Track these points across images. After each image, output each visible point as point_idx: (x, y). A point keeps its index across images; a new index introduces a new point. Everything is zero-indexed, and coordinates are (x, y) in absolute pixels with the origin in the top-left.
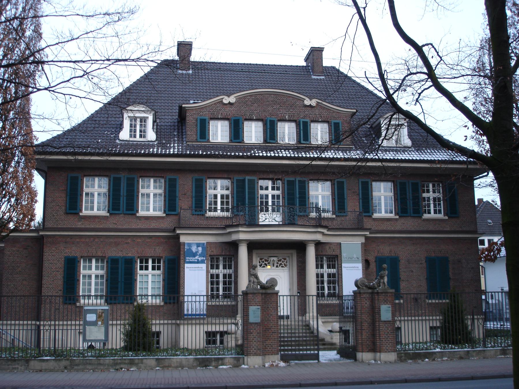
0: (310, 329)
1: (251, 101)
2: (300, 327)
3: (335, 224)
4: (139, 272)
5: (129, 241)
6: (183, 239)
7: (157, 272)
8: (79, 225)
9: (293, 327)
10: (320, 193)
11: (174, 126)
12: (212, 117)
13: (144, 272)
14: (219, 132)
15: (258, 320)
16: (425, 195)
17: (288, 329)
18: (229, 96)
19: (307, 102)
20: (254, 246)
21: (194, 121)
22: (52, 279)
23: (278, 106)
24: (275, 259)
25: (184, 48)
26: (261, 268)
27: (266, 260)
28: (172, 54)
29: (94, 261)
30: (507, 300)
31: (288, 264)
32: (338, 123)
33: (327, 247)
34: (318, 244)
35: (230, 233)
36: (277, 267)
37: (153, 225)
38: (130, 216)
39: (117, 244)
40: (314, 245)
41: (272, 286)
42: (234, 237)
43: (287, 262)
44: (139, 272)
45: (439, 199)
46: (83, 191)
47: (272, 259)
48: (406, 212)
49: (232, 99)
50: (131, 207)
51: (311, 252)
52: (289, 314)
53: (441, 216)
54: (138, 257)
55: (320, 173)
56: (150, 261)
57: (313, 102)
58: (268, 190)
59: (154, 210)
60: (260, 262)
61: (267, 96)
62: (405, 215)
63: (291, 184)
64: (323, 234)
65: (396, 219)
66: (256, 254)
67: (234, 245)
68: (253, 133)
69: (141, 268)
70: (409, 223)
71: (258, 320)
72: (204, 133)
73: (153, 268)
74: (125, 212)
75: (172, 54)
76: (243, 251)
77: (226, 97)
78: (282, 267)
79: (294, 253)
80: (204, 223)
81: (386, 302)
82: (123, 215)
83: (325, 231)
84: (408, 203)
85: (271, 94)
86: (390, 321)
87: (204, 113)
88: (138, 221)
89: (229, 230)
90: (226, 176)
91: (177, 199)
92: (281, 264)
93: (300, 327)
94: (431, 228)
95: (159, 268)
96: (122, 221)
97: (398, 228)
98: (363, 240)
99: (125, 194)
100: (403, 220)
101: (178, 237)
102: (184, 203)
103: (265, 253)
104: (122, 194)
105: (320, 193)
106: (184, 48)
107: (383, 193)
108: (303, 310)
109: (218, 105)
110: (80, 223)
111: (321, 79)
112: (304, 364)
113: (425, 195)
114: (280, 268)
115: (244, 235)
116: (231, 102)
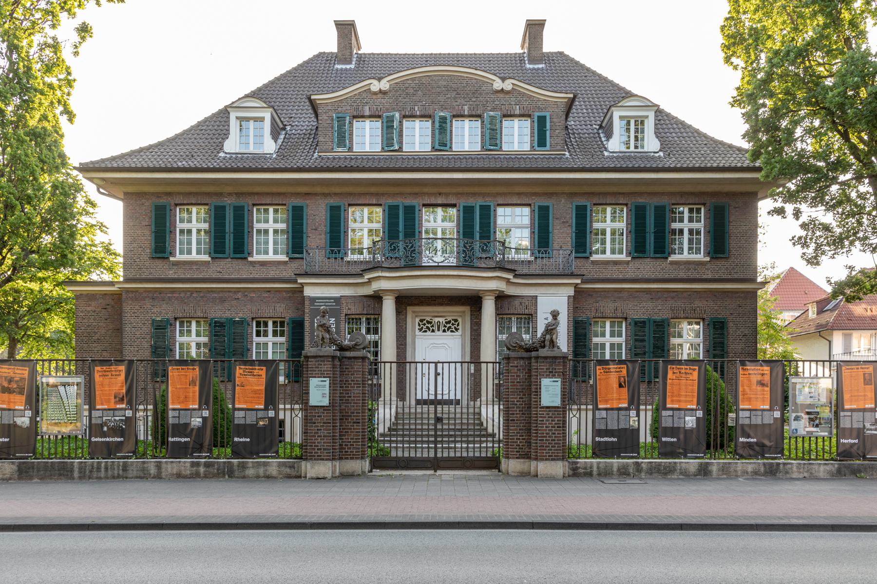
0: (480, 419)
1: (413, 88)
2: (471, 416)
3: (535, 269)
4: (256, 339)
5: (239, 295)
6: (309, 292)
7: (280, 339)
8: (171, 274)
9: (419, 416)
10: (514, 226)
11: (310, 134)
12: (355, 114)
13: (262, 339)
14: (367, 138)
15: (326, 402)
16: (676, 225)
17: (416, 419)
18: (380, 79)
19: (498, 85)
20: (405, 301)
21: (329, 122)
22: (136, 349)
23: (454, 94)
24: (441, 320)
25: (346, 30)
26: (421, 333)
27: (428, 322)
28: (331, 45)
29: (194, 324)
30: (629, 244)
31: (460, 327)
32: (545, 117)
33: (517, 302)
34: (501, 298)
35: (370, 281)
36: (444, 331)
37: (272, 273)
38: (240, 261)
39: (223, 300)
40: (493, 298)
41: (356, 345)
42: (376, 286)
43: (458, 325)
44: (256, 339)
45: (698, 233)
46: (175, 227)
47: (437, 320)
48: (643, 251)
49: (384, 85)
50: (241, 249)
51: (489, 307)
52: (459, 397)
53: (700, 257)
54: (253, 319)
55: (513, 194)
56: (270, 324)
57: (508, 85)
58: (440, 223)
59: (276, 252)
60: (419, 325)
61: (437, 78)
62: (641, 255)
63: (468, 212)
64: (508, 281)
65: (628, 263)
66: (413, 312)
67: (377, 298)
68: (417, 137)
69: (258, 335)
70: (648, 267)
71: (326, 402)
72: (343, 138)
73: (275, 334)
74: (232, 255)
75: (331, 45)
76: (389, 307)
77: (375, 82)
78: (452, 331)
79: (467, 309)
80: (344, 269)
81: (551, 374)
82: (230, 260)
83: (510, 276)
84: (650, 236)
85: (444, 76)
86: (558, 407)
87: (344, 108)
88: (251, 268)
89: (368, 276)
90: (374, 202)
91: (305, 236)
92: (450, 327)
93: (471, 416)
94: (682, 275)
95: (282, 335)
96: (228, 267)
97: (630, 275)
98: (571, 291)
99: (232, 230)
100: (638, 263)
101: (300, 290)
102: (316, 241)
103: (427, 312)
104: (227, 230)
105: (514, 226)
106: (346, 30)
107: (611, 224)
108: (475, 392)
109: (364, 95)
110: (171, 272)
111: (538, 69)
112: (405, 478)
113: (676, 225)
114: (449, 333)
115: (390, 283)
116: (383, 89)
